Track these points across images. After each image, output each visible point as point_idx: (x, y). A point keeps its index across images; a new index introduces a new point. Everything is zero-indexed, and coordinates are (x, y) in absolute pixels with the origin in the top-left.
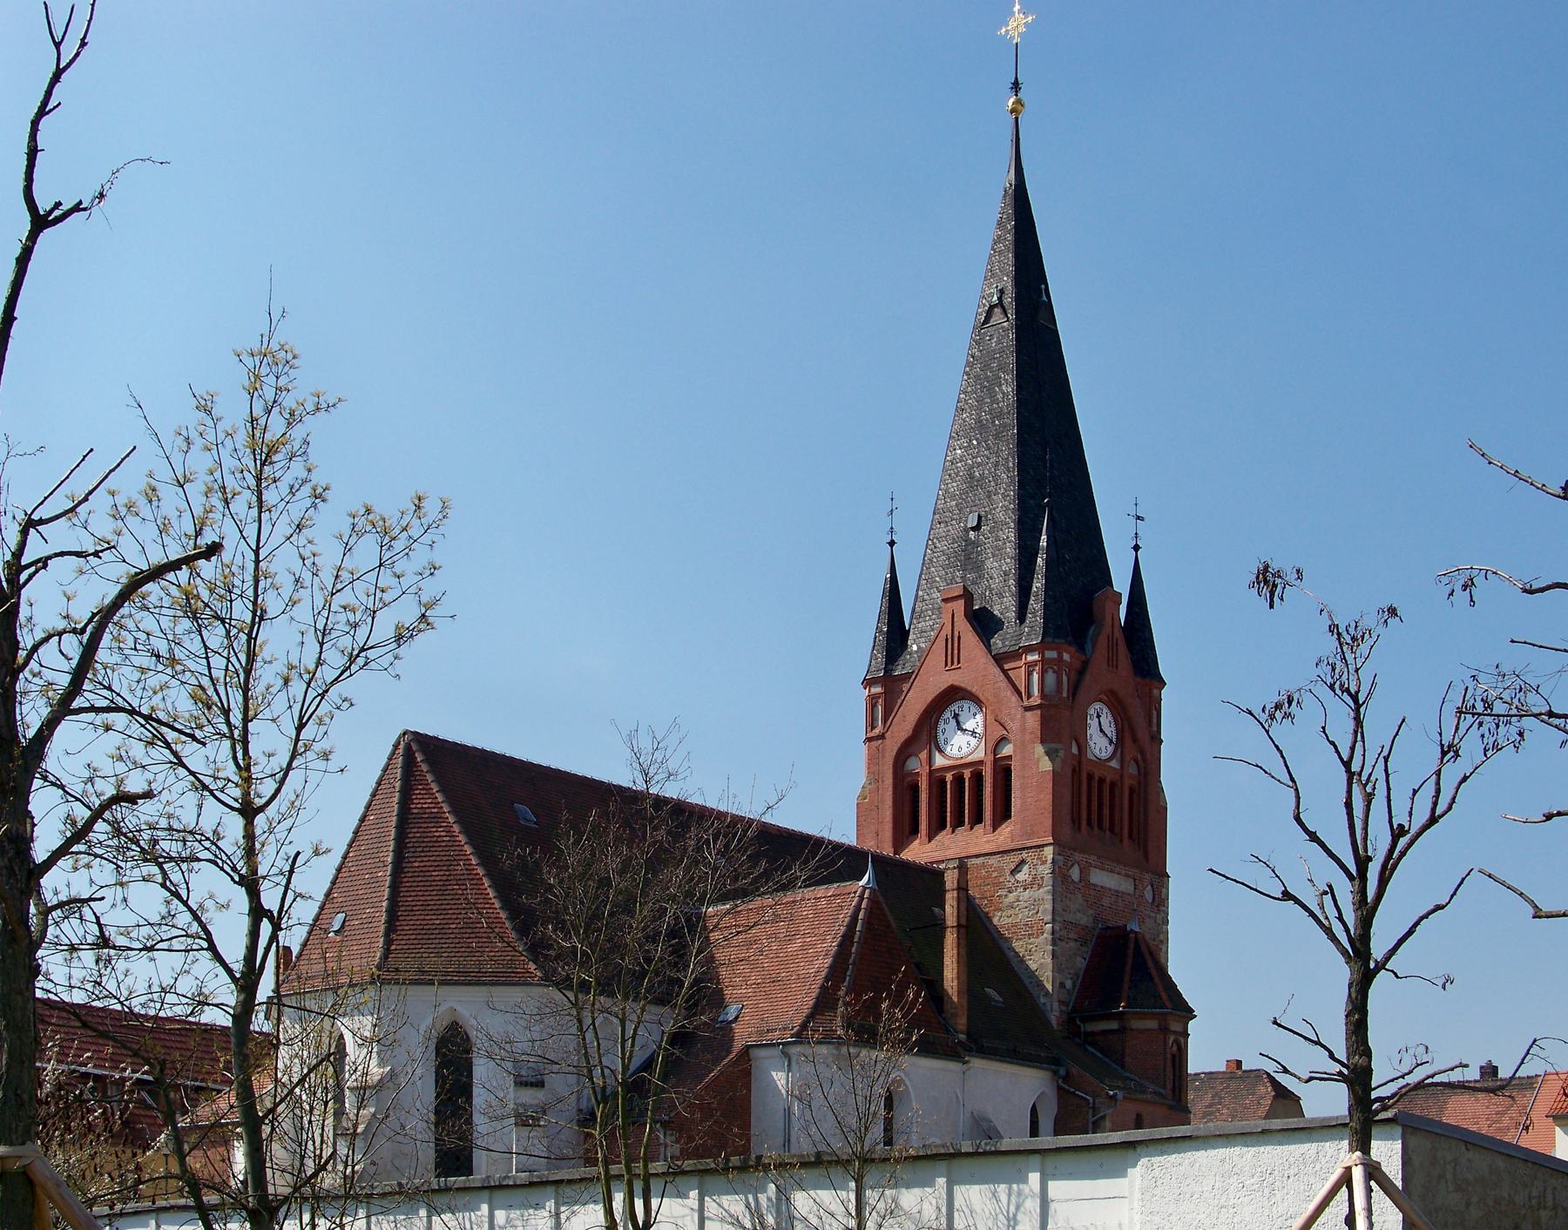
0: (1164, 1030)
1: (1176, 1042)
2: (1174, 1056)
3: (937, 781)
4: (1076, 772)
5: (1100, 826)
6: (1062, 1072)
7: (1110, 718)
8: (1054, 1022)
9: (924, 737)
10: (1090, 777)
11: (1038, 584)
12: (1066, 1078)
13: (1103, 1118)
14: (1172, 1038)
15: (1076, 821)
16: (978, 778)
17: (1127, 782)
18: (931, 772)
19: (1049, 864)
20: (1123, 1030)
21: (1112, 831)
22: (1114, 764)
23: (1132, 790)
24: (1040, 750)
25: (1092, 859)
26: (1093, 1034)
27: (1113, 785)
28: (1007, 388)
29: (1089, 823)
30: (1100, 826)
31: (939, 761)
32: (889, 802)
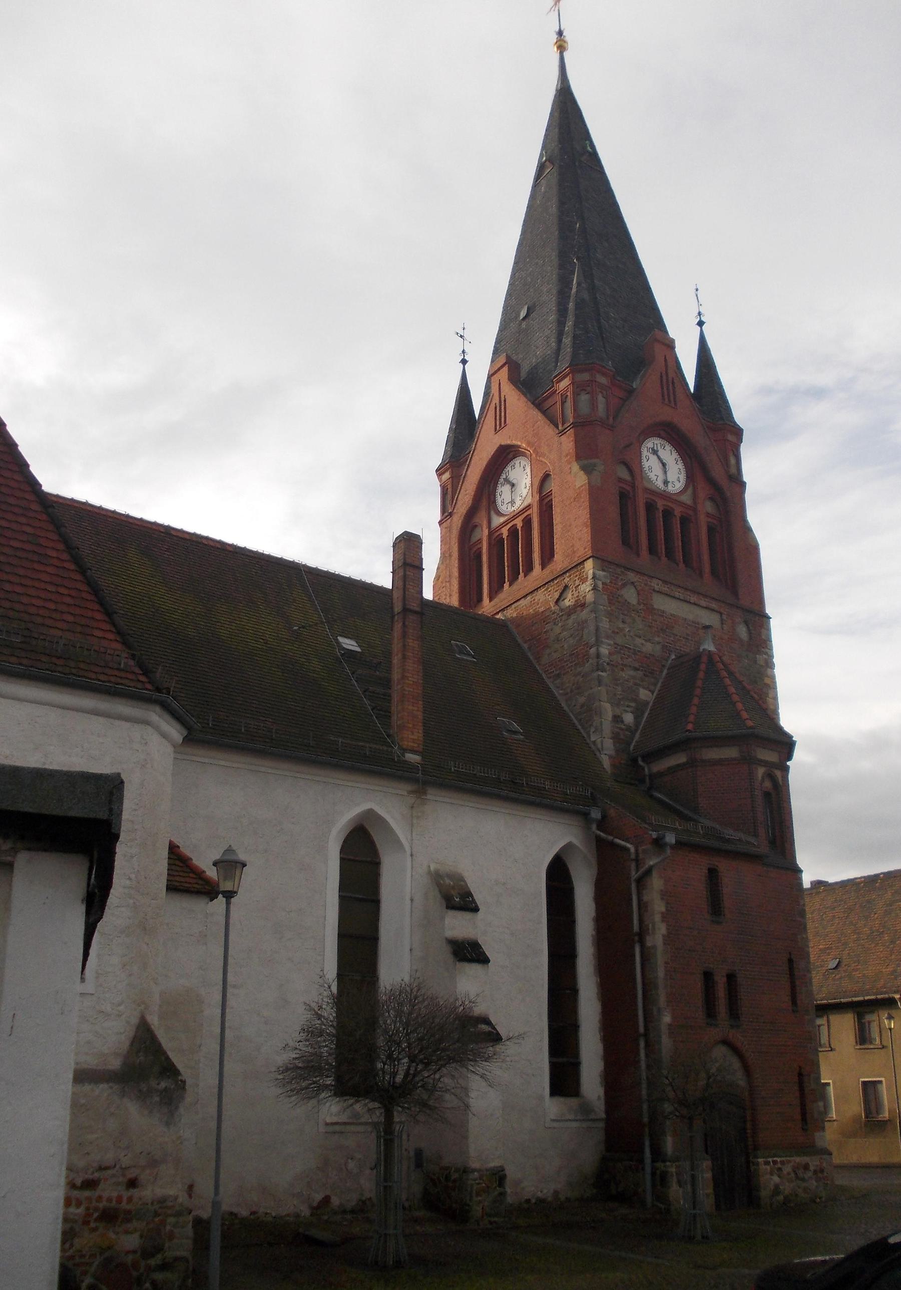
0: (749, 761)
1: (771, 777)
2: (767, 795)
3: (496, 542)
4: (625, 498)
5: (669, 553)
6: (596, 814)
7: (668, 447)
8: (606, 763)
9: (484, 503)
10: (650, 507)
11: (570, 324)
12: (602, 824)
13: (649, 872)
14: (761, 771)
15: (627, 540)
16: (528, 522)
17: (703, 521)
18: (491, 534)
19: (590, 581)
20: (693, 763)
21: (686, 562)
22: (686, 499)
23: (711, 530)
24: (575, 467)
25: (656, 584)
26: (661, 774)
27: (685, 521)
28: (554, 209)
29: (652, 550)
30: (669, 553)
31: (497, 521)
32: (456, 573)
